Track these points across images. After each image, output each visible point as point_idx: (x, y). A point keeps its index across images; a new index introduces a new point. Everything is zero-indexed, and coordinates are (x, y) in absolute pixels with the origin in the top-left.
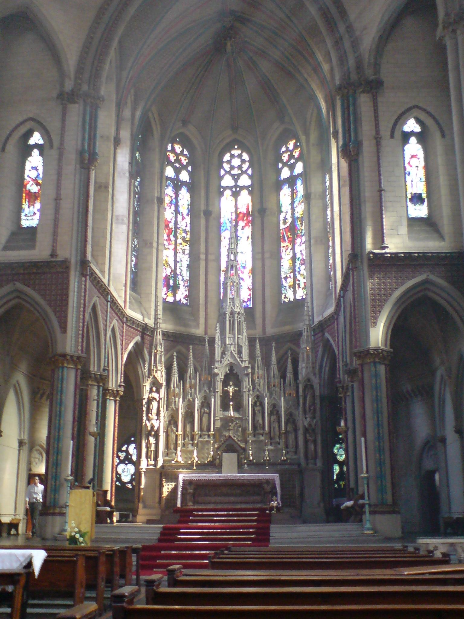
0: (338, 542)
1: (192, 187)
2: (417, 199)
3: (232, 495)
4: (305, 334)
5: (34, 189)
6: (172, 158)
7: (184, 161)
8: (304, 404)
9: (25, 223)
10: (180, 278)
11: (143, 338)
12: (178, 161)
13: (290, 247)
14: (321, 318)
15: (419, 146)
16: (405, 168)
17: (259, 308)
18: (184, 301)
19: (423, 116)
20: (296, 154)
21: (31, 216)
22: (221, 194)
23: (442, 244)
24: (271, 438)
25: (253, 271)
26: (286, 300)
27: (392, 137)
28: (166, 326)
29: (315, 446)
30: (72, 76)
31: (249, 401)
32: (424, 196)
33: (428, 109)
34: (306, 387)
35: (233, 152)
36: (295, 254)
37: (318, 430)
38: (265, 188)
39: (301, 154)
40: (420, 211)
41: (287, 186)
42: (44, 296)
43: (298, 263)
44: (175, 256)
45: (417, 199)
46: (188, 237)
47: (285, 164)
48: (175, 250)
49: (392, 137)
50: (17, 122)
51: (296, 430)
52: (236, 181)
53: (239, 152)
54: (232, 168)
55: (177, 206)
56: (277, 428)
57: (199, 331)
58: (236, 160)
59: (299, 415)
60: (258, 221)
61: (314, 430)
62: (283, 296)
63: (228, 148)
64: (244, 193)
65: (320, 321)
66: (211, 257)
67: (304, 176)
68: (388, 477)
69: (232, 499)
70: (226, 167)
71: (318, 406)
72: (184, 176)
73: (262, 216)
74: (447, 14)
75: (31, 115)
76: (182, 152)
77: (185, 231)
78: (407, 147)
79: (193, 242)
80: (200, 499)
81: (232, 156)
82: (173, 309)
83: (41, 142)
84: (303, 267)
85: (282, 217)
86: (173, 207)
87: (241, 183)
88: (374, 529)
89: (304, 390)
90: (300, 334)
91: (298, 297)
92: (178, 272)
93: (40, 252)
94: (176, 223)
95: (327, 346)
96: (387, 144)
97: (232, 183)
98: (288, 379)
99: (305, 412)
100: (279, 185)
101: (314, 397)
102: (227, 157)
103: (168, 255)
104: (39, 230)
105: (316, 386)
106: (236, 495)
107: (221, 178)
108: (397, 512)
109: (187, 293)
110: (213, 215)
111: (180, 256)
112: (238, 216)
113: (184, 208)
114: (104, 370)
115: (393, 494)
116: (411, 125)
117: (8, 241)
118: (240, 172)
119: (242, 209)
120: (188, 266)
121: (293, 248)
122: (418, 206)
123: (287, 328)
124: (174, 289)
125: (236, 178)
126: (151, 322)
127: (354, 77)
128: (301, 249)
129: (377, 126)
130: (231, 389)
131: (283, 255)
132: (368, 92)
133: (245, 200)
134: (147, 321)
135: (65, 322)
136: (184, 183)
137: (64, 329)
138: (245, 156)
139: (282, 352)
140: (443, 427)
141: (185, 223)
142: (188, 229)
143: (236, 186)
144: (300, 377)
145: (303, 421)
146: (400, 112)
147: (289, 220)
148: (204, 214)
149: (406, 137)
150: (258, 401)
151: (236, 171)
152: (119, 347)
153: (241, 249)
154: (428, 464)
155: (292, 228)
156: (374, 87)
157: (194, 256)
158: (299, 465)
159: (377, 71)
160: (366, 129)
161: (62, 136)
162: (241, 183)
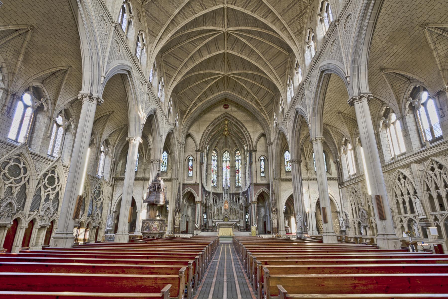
1: (217, 161)
2: (263, 172)
6: (213, 154)
7: (216, 155)
17: (231, 187)
20: (239, 154)
22: (223, 162)
25: (230, 179)
28: (213, 191)
40: (263, 175)
58: (226, 155)
63: (225, 152)
64: (228, 162)
67: (241, 160)
72: (216, 158)
73: (232, 167)
79: (217, 173)
90: (240, 193)
93: (193, 182)
96: (258, 163)
102: (224, 154)
112: (227, 167)
113: (215, 165)
123: (237, 192)
124: (214, 183)
125: (226, 158)
127: (252, 149)
138: (228, 154)
141: (216, 169)
145: (240, 212)
149: (261, 160)
152: (144, 151)
153: (226, 173)
154: (264, 220)
155: (238, 170)
157: (218, 176)
159: (256, 148)
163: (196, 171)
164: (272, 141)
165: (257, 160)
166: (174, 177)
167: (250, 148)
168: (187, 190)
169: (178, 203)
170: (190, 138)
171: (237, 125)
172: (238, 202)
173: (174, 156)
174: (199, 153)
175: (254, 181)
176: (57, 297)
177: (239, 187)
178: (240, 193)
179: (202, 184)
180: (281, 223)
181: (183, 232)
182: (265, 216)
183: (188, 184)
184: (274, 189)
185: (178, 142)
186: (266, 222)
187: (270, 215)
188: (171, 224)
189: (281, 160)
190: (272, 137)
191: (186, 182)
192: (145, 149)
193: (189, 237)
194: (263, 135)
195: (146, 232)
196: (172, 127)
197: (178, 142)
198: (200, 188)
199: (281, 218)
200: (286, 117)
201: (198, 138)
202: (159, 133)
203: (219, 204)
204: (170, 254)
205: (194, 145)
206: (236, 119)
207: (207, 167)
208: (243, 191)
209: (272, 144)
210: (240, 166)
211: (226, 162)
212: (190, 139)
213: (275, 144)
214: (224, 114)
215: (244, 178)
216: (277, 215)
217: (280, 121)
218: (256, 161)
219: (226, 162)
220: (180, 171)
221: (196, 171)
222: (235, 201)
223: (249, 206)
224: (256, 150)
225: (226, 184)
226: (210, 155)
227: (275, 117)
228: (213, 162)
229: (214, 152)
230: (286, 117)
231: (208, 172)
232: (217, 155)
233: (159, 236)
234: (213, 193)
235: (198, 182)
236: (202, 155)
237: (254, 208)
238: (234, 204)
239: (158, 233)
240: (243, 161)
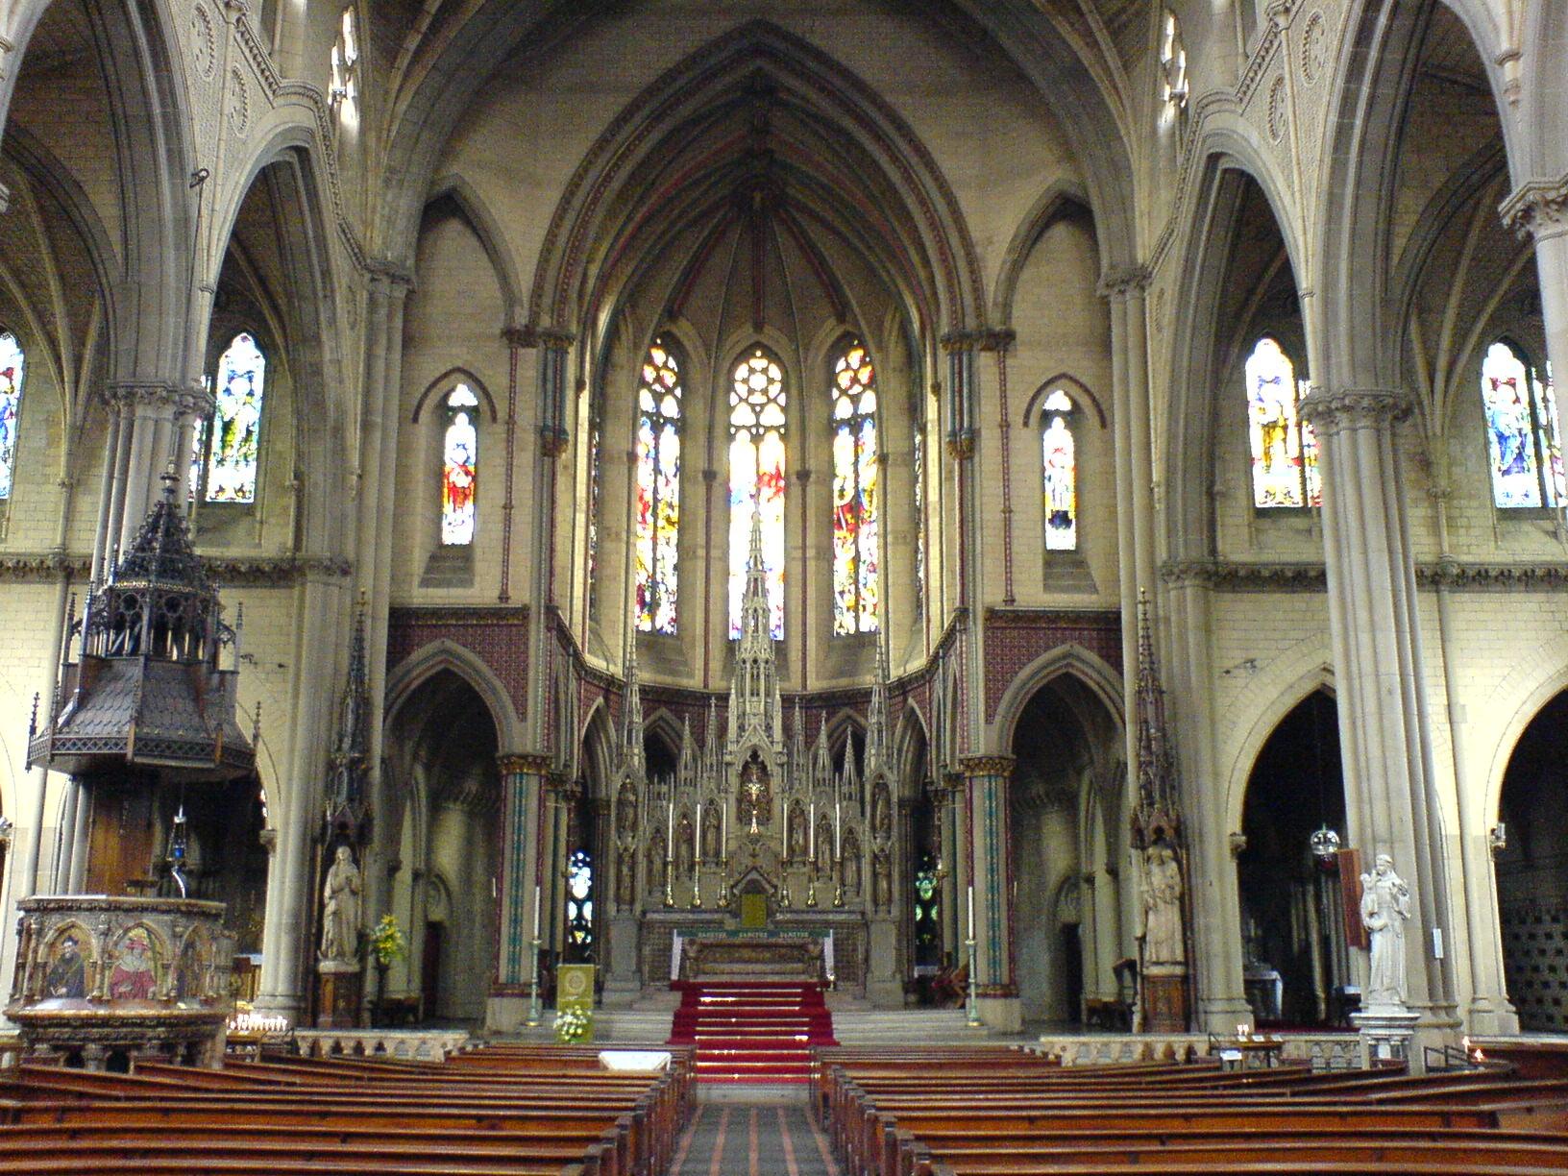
0: (288, 806)
1: (682, 427)
2: (1061, 519)
3: (757, 961)
4: (875, 699)
5: (462, 481)
6: (649, 374)
7: (670, 379)
8: (873, 816)
9: (448, 538)
10: (662, 588)
11: (606, 699)
12: (659, 379)
13: (851, 539)
14: (901, 672)
15: (1068, 434)
16: (1044, 469)
17: (795, 644)
18: (669, 629)
19: (1075, 391)
20: (864, 375)
21: (459, 526)
22: (731, 438)
23: (1094, 597)
24: (818, 870)
25: (786, 578)
26: (843, 632)
27: (1026, 424)
28: (645, 676)
29: (890, 884)
30: (526, 300)
31: (782, 808)
32: (1071, 515)
33: (1084, 380)
34: (876, 786)
35: (753, 363)
36: (857, 552)
37: (896, 858)
38: (809, 428)
39: (873, 378)
40: (1062, 539)
41: (847, 430)
42: (489, 663)
43: (863, 569)
44: (654, 550)
45: (1061, 519)
46: (675, 516)
47: (844, 392)
48: (655, 539)
49: (1026, 424)
50: (437, 374)
51: (858, 857)
52: (758, 415)
53: (764, 363)
54: (751, 391)
55: (656, 460)
56: (827, 855)
57: (694, 683)
59: (863, 832)
60: (796, 491)
61: (888, 858)
62: (837, 624)
63: (745, 355)
64: (772, 437)
65: (900, 679)
66: (714, 553)
67: (877, 418)
68: (1005, 945)
69: (759, 967)
70: (741, 388)
71: (895, 821)
72: (670, 408)
74: (1112, 267)
75: (459, 363)
76: (665, 364)
77: (671, 506)
78: (1048, 435)
80: (708, 966)
81: (752, 371)
82: (652, 643)
83: (473, 402)
84: (874, 576)
85: (837, 485)
86: (651, 462)
87: (765, 420)
88: (982, 1023)
89: (873, 795)
90: (867, 694)
91: (864, 628)
92: (659, 577)
93: (482, 592)
94: (655, 491)
95: (912, 719)
96: (1021, 436)
97: (751, 420)
98: (846, 774)
99: (873, 828)
100: (832, 428)
101: (888, 802)
102: (742, 371)
103: (643, 548)
104: (478, 553)
105: (893, 787)
106: (763, 962)
107: (730, 409)
108: (1017, 996)
109: (673, 614)
110: (719, 479)
111: (662, 549)
114: (566, 766)
115: (1011, 971)
116: (1058, 401)
117: (428, 570)
118: (764, 400)
119: (768, 468)
120: (676, 568)
121: (856, 542)
122: (1061, 531)
123: (843, 682)
124: (652, 607)
125: (757, 410)
126: (617, 670)
128: (869, 542)
129: (1004, 406)
130: (754, 789)
131: (838, 551)
132: (990, 349)
133: (774, 453)
134: (612, 668)
135: (525, 707)
136: (668, 420)
137: (522, 716)
138: (775, 372)
139: (835, 720)
140: (1091, 854)
141: (670, 492)
142: (676, 503)
143: (758, 425)
144: (867, 772)
145: (869, 844)
146: (1039, 384)
147: (849, 494)
148: (705, 482)
149: (1047, 417)
150: (797, 813)
151: (758, 398)
152: (62, 334)
154: (1067, 914)
155: (855, 507)
156: (1001, 341)
158: (863, 914)
159: (1007, 317)
160: (988, 413)
161: (512, 400)
162: (765, 420)
163: (508, 507)
164: (1142, 255)
165: (1016, 419)
166: (317, 545)
167: (958, 316)
168: (424, 658)
169: (340, 771)
170: (453, 228)
171: (848, 123)
172: (848, 765)
173: (317, 371)
174: (530, 358)
175: (989, 594)
176: (207, 1171)
177: (861, 642)
178: (867, 694)
179: (551, 611)
180: (1216, 938)
181: (393, 1015)
182: (1076, 881)
183: (437, 613)
184: (1169, 656)
185: (358, 254)
186: (1085, 933)
187: (1113, 871)
188: (285, 941)
189: (1215, 416)
190: (1141, 224)
191: (421, 596)
192: (71, 314)
193: (437, 1055)
194: (1070, 210)
195: (50, 1007)
196: (302, 117)
197: (358, 254)
198: (538, 637)
199: (1214, 893)
200: (1274, 31)
201: (523, 223)
202: (177, 156)
203: (692, 783)
204: (423, 1105)
205: (488, 288)
206: (846, 73)
207: (597, 480)
208: (895, 673)
209: (1139, 278)
210: (870, 474)
211: (757, 439)
212: (453, 236)
213: (1167, 278)
214: (742, 32)
215: (898, 564)
216: (1185, 874)
217: (1217, 74)
218: (1005, 425)
219: (757, 439)
220: (371, 500)
221: (508, 507)
222: (824, 757)
223: (941, 795)
224: (1009, 336)
225: (756, 614)
226: (620, 380)
227: (1167, 54)
228: (645, 434)
229: (659, 356)
230: (1274, 31)
231: (610, 520)
232: (682, 379)
233: (167, 1047)
234: (644, 691)
235: (521, 594)
236: (560, 371)
237: (976, 824)
238: (816, 783)
239: (160, 1022)
240: (897, 428)
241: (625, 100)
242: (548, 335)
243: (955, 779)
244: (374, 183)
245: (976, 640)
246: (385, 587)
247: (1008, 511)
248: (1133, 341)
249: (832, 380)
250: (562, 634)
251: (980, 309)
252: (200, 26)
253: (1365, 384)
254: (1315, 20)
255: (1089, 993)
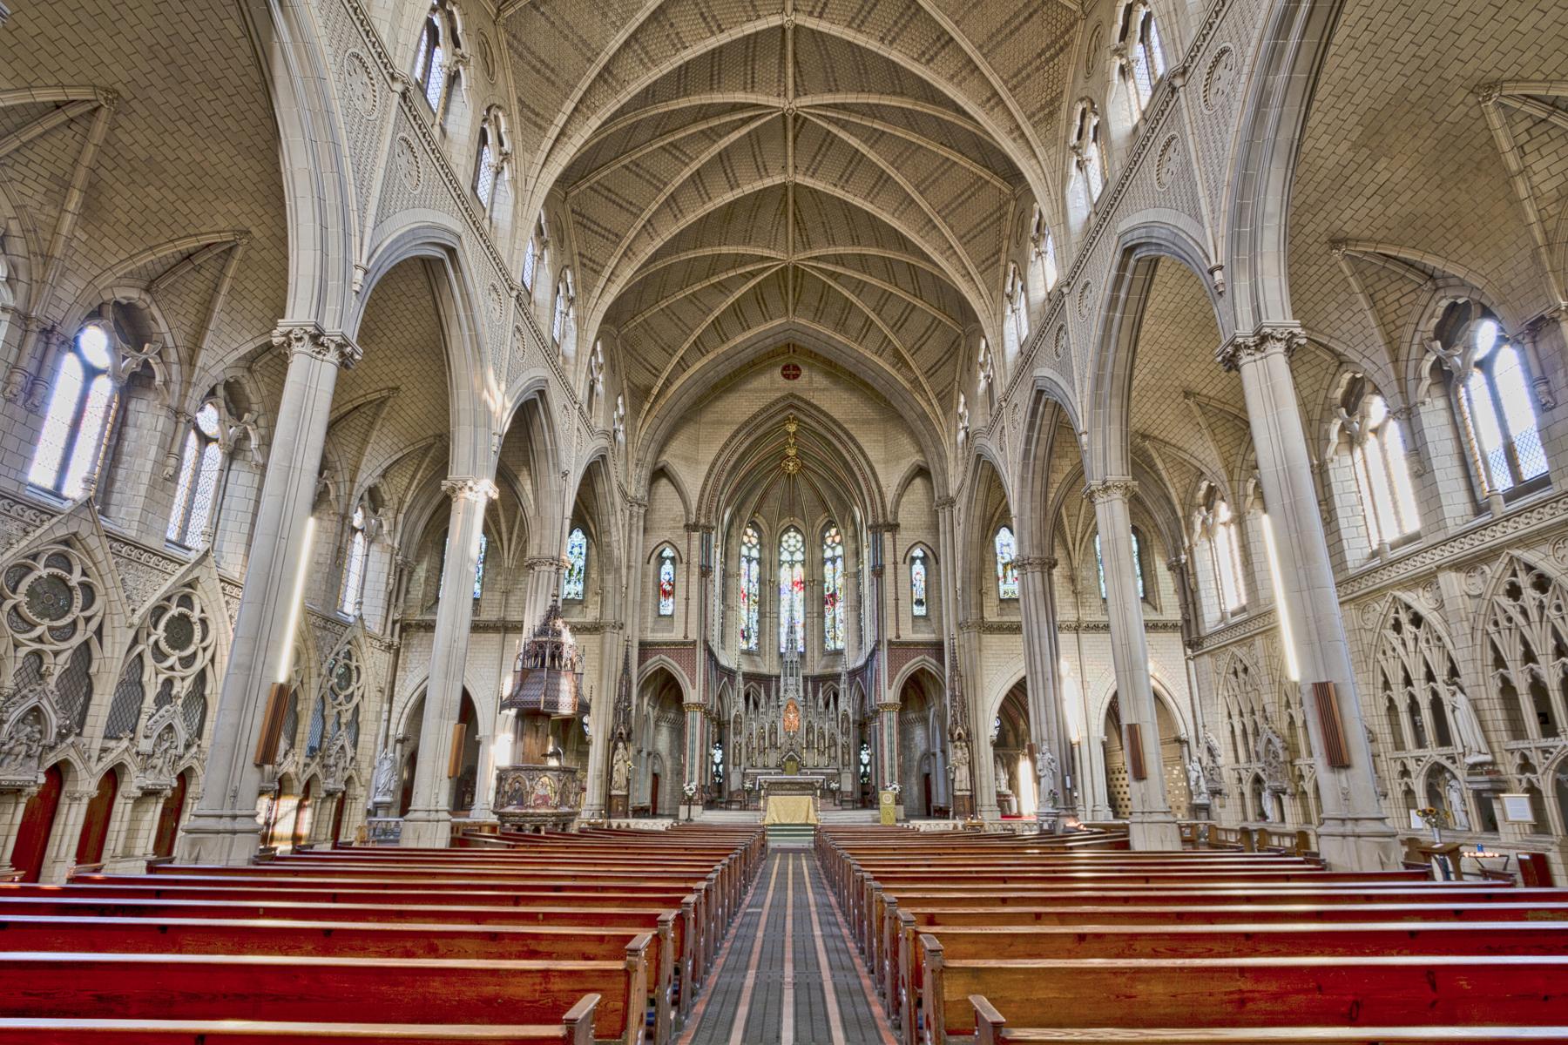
1: (760, 562)
2: (920, 602)
6: (746, 539)
7: (754, 541)
17: (809, 654)
20: (837, 539)
22: (780, 566)
40: (920, 611)
58: (792, 541)
63: (787, 530)
64: (798, 567)
67: (844, 558)
72: (755, 553)
73: (813, 585)
79: (761, 604)
90: (839, 675)
93: (677, 635)
102: (785, 537)
112: (794, 584)
113: (754, 578)
123: (829, 670)
124: (748, 638)
125: (792, 553)
127: (881, 520)
138: (799, 537)
141: (755, 589)
145: (840, 740)
149: (913, 560)
152: (504, 529)
153: (792, 604)
154: (926, 769)
155: (833, 595)
157: (762, 615)
163: (687, 599)
164: (952, 493)
165: (900, 560)
166: (609, 617)
167: (875, 517)
168: (653, 663)
169: (621, 710)
170: (664, 481)
172: (832, 705)
173: (609, 545)
174: (696, 535)
175: (890, 634)
177: (838, 653)
178: (839, 675)
179: (706, 642)
180: (984, 780)
181: (641, 812)
182: (928, 755)
184: (961, 659)
185: (624, 495)
186: (932, 777)
187: (944, 752)
188: (597, 782)
190: (951, 480)
191: (650, 637)
193: (662, 829)
194: (922, 472)
195: (510, 809)
197: (624, 495)
198: (700, 655)
199: (983, 760)
200: (1001, 408)
201: (693, 480)
202: (556, 465)
203: (765, 713)
205: (678, 508)
207: (724, 585)
208: (851, 666)
209: (951, 502)
210: (840, 582)
212: (664, 486)
213: (961, 503)
214: (783, 398)
215: (853, 620)
216: (971, 753)
217: (980, 422)
218: (895, 563)
219: (792, 566)
220: (630, 598)
221: (687, 599)
222: (821, 702)
223: (870, 719)
224: (898, 525)
225: (792, 641)
226: (734, 542)
227: (961, 409)
228: (744, 564)
229: (750, 531)
232: (760, 543)
233: (556, 825)
234: (745, 675)
235: (693, 636)
236: (708, 541)
237: (887, 728)
240: (851, 562)
241: (735, 427)
242: (704, 527)
243: (877, 712)
244: (631, 466)
245: (883, 656)
246: (637, 633)
247: (897, 599)
248: (948, 528)
249: (823, 539)
250: (711, 654)
251: (884, 515)
252: (494, 295)
253: (1036, 554)
254: (1087, 284)
255: (934, 803)
